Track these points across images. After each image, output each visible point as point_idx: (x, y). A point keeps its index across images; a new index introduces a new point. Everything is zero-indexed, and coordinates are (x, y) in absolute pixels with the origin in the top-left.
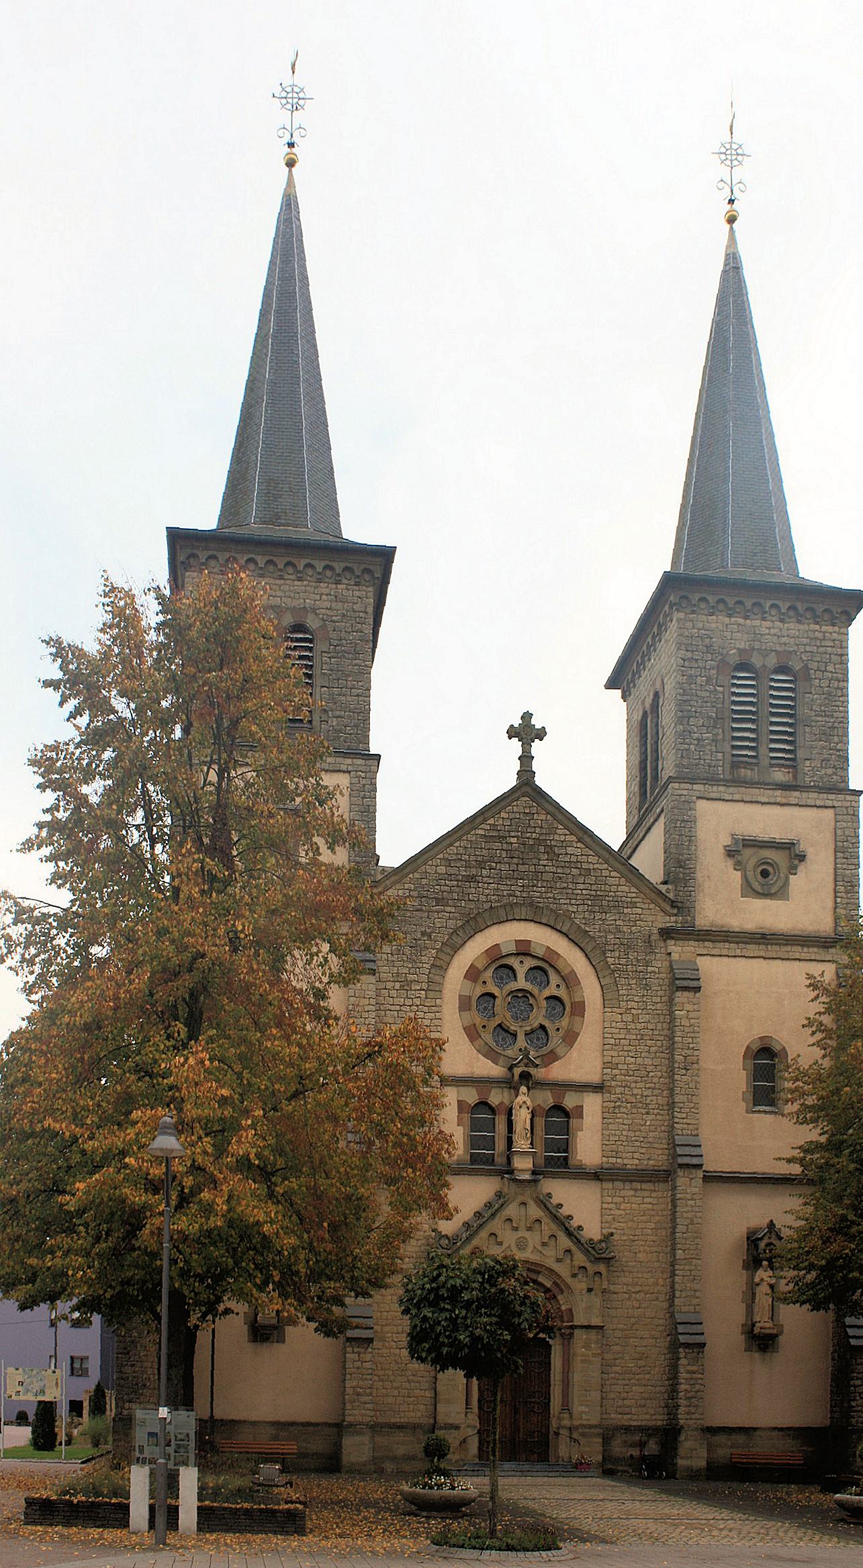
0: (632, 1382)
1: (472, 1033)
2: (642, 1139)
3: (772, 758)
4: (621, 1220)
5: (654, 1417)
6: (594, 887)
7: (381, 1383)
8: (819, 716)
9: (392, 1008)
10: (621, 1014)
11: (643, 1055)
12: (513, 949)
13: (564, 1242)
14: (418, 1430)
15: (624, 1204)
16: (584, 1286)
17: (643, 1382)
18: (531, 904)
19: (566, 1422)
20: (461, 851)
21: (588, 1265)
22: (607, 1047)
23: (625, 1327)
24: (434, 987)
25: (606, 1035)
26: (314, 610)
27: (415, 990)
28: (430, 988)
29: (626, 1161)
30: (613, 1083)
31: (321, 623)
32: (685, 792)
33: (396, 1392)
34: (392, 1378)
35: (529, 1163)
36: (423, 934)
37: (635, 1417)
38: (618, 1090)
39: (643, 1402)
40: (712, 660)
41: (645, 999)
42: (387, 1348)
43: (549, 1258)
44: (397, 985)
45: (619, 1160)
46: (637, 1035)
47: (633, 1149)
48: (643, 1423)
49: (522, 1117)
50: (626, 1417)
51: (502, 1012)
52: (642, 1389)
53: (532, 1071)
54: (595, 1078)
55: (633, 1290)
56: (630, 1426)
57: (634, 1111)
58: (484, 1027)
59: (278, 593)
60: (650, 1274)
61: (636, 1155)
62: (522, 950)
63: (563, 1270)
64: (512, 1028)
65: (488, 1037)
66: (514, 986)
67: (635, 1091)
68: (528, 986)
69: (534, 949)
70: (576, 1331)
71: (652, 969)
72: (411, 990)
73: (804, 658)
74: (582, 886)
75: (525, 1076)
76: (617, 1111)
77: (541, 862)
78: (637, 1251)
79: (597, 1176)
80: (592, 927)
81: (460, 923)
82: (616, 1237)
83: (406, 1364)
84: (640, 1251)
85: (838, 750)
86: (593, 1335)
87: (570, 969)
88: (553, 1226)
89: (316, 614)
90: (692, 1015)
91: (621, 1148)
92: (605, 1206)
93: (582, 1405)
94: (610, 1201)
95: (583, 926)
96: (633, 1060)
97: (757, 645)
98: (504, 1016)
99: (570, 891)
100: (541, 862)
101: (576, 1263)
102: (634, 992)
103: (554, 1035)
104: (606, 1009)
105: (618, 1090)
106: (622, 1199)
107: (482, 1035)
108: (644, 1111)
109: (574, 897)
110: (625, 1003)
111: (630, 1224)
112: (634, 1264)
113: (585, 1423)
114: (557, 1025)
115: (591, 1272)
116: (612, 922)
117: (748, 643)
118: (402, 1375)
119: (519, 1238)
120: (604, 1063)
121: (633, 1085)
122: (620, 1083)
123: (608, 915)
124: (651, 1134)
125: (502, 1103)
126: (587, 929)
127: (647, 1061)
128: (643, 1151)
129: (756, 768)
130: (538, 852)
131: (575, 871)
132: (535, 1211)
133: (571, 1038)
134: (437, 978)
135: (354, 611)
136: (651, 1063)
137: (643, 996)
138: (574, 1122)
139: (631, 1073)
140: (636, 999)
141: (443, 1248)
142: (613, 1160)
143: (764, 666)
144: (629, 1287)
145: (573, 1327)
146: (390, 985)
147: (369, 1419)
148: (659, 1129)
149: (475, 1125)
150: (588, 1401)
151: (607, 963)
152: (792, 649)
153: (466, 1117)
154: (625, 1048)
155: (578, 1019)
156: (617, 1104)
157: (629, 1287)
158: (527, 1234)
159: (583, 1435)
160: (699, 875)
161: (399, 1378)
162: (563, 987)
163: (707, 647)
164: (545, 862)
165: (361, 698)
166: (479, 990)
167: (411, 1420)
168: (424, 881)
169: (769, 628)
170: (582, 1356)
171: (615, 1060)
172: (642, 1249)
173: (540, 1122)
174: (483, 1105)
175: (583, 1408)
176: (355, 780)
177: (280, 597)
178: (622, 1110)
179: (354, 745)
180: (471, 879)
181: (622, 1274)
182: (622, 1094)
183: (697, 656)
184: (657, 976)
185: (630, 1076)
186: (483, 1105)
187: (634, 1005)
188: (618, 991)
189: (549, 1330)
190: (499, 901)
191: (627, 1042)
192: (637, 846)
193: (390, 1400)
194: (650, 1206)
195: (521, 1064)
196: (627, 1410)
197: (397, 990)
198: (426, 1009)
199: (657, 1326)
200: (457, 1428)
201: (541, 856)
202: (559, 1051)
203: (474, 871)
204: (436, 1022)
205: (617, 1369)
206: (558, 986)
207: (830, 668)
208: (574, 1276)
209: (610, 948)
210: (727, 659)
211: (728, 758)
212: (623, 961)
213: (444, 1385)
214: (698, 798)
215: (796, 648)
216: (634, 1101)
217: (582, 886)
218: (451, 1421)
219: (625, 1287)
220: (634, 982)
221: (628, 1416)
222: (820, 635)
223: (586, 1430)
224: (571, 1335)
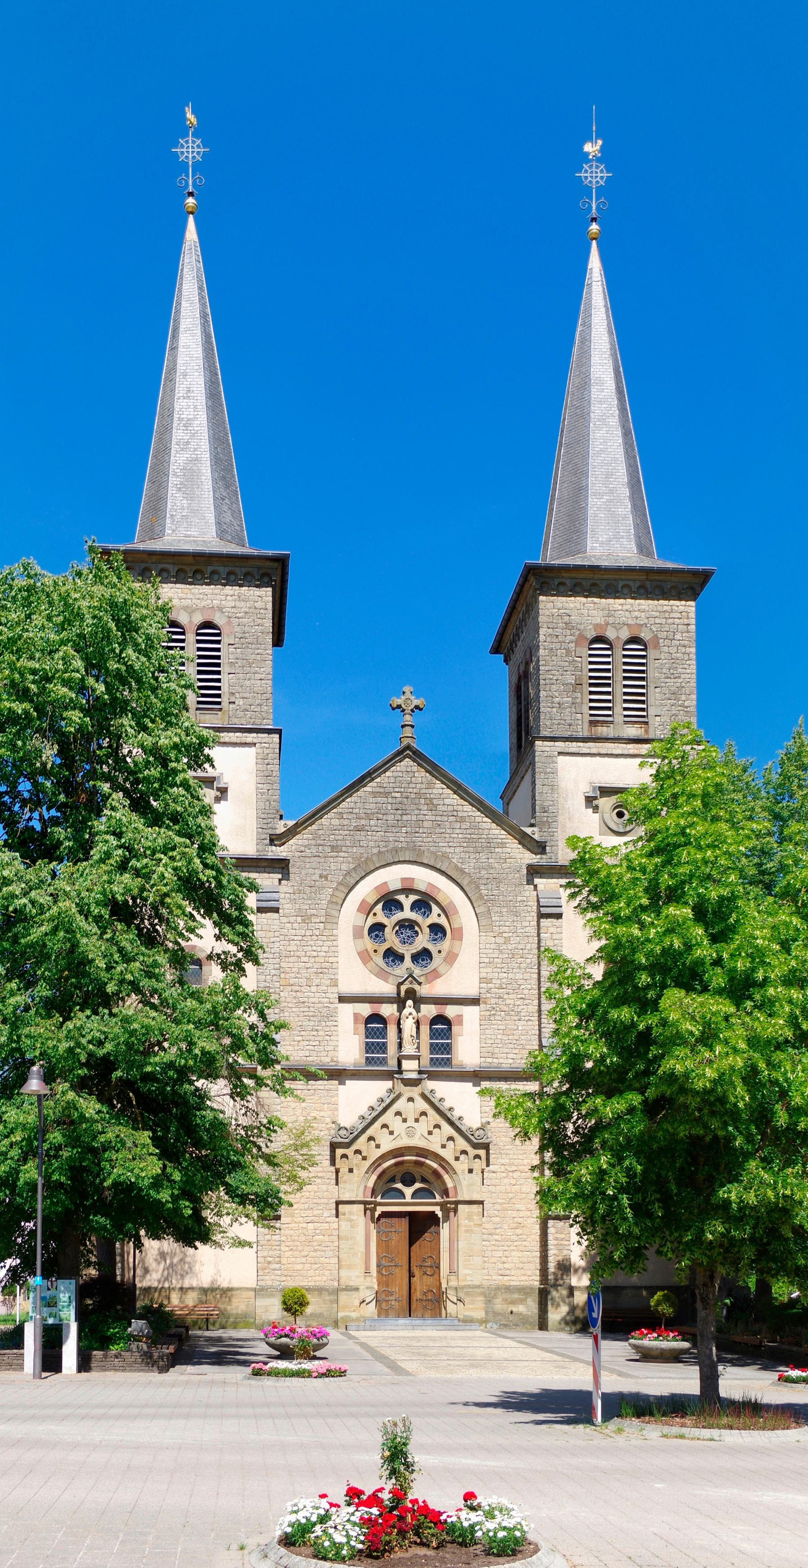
1: (365, 956)
3: (626, 716)
5: (531, 1278)
6: (469, 831)
7: (291, 1253)
8: (668, 678)
9: (296, 938)
11: (515, 971)
12: (399, 886)
13: (448, 1130)
14: (324, 1292)
16: (466, 1167)
17: (521, 1248)
18: (414, 849)
19: (453, 1283)
20: (352, 805)
22: (482, 965)
24: (331, 920)
25: (482, 955)
26: (220, 609)
29: (501, 1061)
30: (488, 995)
31: (227, 620)
32: (548, 749)
33: (304, 1260)
36: (321, 876)
37: (514, 1278)
38: (493, 1001)
40: (571, 635)
43: (434, 1144)
44: (299, 919)
45: (495, 1060)
48: (522, 1283)
49: (409, 1026)
50: (506, 1278)
51: (392, 939)
53: (416, 987)
54: (472, 991)
58: (375, 951)
59: (190, 596)
61: (510, 1056)
62: (407, 886)
63: (448, 1154)
64: (400, 951)
65: (379, 959)
66: (399, 916)
67: (508, 1002)
70: (460, 1206)
73: (654, 629)
74: (458, 831)
75: (411, 994)
76: (492, 1018)
77: (422, 812)
79: (476, 1076)
81: (352, 866)
85: (687, 707)
86: (476, 1208)
87: (448, 901)
89: (222, 612)
90: (555, 936)
91: (497, 1050)
95: (459, 865)
96: (505, 975)
97: (611, 620)
99: (447, 836)
100: (422, 812)
105: (493, 1001)
107: (374, 958)
108: (516, 1018)
109: (451, 840)
110: (497, 928)
113: (470, 1283)
114: (439, 948)
117: (603, 619)
121: (506, 996)
124: (523, 1037)
127: (519, 976)
128: (515, 1051)
129: (612, 725)
130: (419, 804)
131: (452, 819)
132: (422, 1105)
133: (451, 958)
134: (334, 913)
135: (255, 608)
136: (521, 977)
140: (507, 924)
142: (490, 1060)
143: (618, 638)
145: (457, 1203)
146: (292, 919)
147: (278, 1283)
149: (369, 1033)
152: (642, 622)
155: (457, 943)
159: (467, 1294)
160: (560, 818)
163: (566, 623)
164: (425, 812)
165: (263, 682)
166: (371, 921)
167: (317, 1284)
168: (321, 832)
169: (622, 605)
171: (490, 976)
173: (425, 1029)
174: (375, 1018)
175: (467, 1271)
176: (260, 751)
177: (191, 599)
178: (497, 1018)
179: (258, 721)
180: (358, 829)
183: (558, 631)
186: (375, 1018)
189: (306, 1145)
190: (386, 846)
191: (499, 961)
192: (516, 791)
193: (300, 1267)
195: (407, 982)
200: (357, 1289)
201: (421, 807)
202: (441, 970)
203: (363, 822)
204: (333, 949)
207: (678, 637)
208: (457, 1159)
210: (584, 633)
211: (587, 718)
214: (560, 753)
215: (646, 621)
217: (458, 831)
218: (351, 1283)
220: (505, 910)
222: (668, 608)
224: (456, 1211)
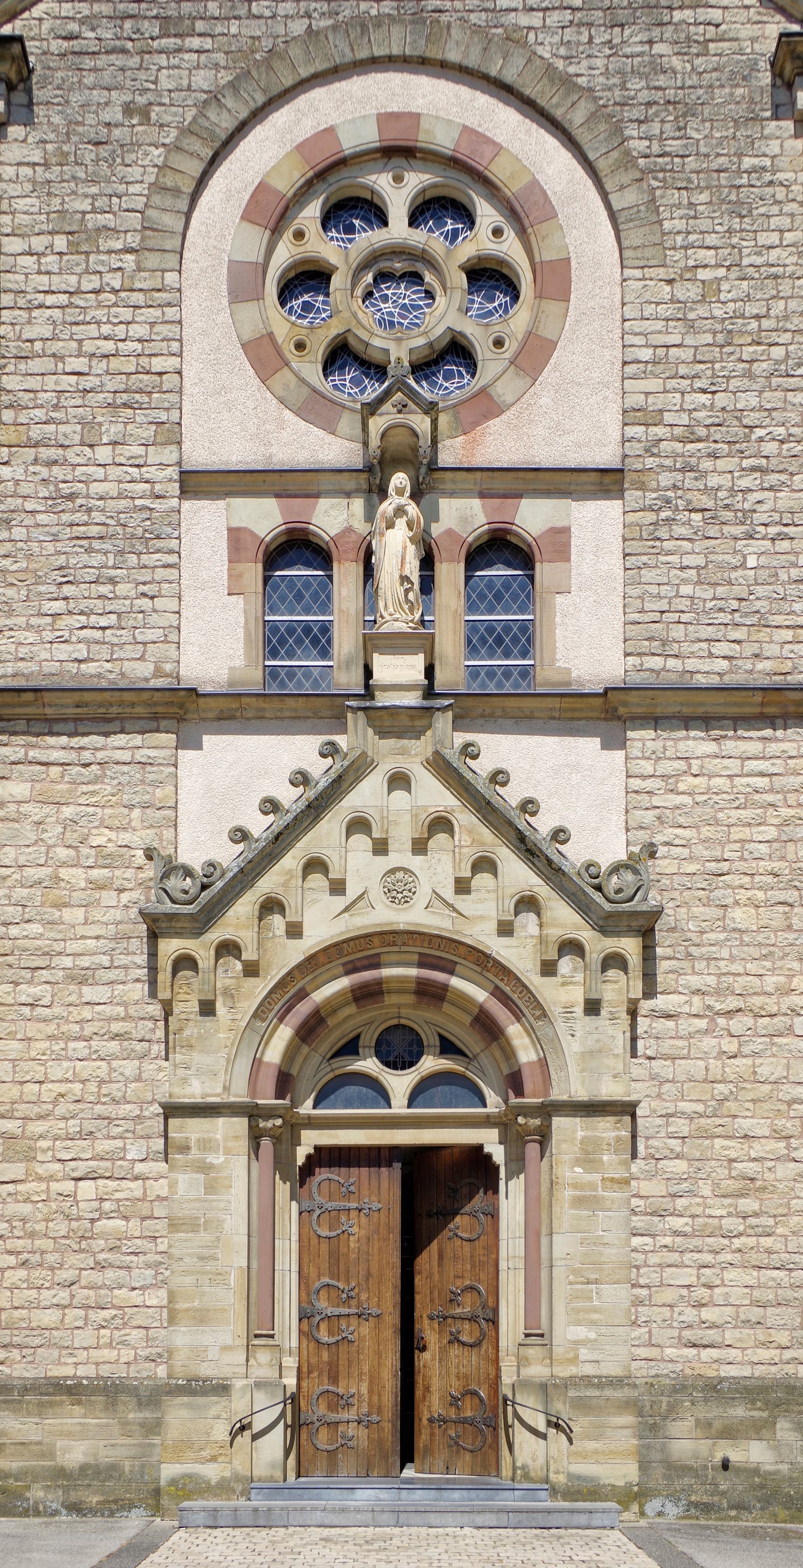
0: (722, 1257)
2: (735, 604)
4: (682, 820)
7: (22, 1273)
9: (50, 300)
10: (670, 282)
15: (690, 779)
16: (577, 995)
17: (755, 1258)
19: (537, 1371)
21: (586, 935)
22: (630, 369)
23: (700, 1108)
27: (110, 252)
28: (150, 244)
29: (692, 664)
30: (650, 462)
34: (51, 1258)
35: (413, 667)
36: (128, 110)
38: (666, 480)
39: (755, 1313)
41: (735, 240)
42: (40, 1179)
44: (60, 243)
45: (672, 663)
46: (715, 333)
47: (709, 633)
48: (759, 1371)
50: (707, 1354)
52: (751, 1277)
55: (718, 1006)
56: (722, 1380)
57: (713, 531)
60: (768, 964)
67: (713, 481)
68: (418, 237)
69: (427, 132)
70: (558, 1122)
71: (756, 161)
72: (99, 252)
78: (729, 901)
80: (585, 63)
81: (225, 77)
82: (663, 864)
83: (93, 1221)
84: (737, 903)
87: (525, 180)
88: (486, 834)
91: (678, 632)
92: (636, 784)
93: (578, 1323)
94: (650, 770)
95: (560, 64)
96: (704, 398)
98: (355, 315)
101: (555, 933)
102: (704, 224)
103: (489, 355)
104: (628, 272)
105: (666, 480)
106: (681, 765)
108: (738, 530)
110: (678, 255)
111: (706, 832)
112: (722, 936)
114: (497, 329)
115: (594, 955)
116: (638, 49)
118: (82, 1251)
119: (393, 871)
120: (625, 411)
121: (707, 464)
122: (668, 462)
123: (627, 32)
124: (760, 591)
125: (349, 530)
126: (572, 70)
137: (729, 231)
138: (543, 571)
139: (702, 432)
140: (711, 240)
141: (173, 901)
142: (656, 662)
144: (710, 1001)
146: (38, 243)
148: (783, 576)
150: (596, 1310)
151: (627, 153)
153: (254, 571)
154: (683, 369)
155: (551, 307)
156: (663, 515)
157: (710, 1001)
158: (415, 863)
161: (73, 1259)
162: (510, 234)
170: (575, 1186)
172: (742, 895)
175: (581, 1332)
178: (679, 531)
181: (686, 964)
182: (675, 487)
184: (768, 177)
185: (699, 440)
187: (708, 256)
188: (660, 222)
193: (50, 1317)
194: (761, 782)
196: (712, 1335)
197: (60, 254)
198: (138, 298)
199: (789, 1103)
200: (223, 1389)
205: (678, 1223)
206: (497, 232)
209: (636, 114)
212: (673, 146)
213: (186, 1273)
216: (710, 504)
218: (206, 1370)
219: (696, 999)
220: (704, 197)
221: (714, 1353)
223: (590, 1393)
224: (544, 1137)
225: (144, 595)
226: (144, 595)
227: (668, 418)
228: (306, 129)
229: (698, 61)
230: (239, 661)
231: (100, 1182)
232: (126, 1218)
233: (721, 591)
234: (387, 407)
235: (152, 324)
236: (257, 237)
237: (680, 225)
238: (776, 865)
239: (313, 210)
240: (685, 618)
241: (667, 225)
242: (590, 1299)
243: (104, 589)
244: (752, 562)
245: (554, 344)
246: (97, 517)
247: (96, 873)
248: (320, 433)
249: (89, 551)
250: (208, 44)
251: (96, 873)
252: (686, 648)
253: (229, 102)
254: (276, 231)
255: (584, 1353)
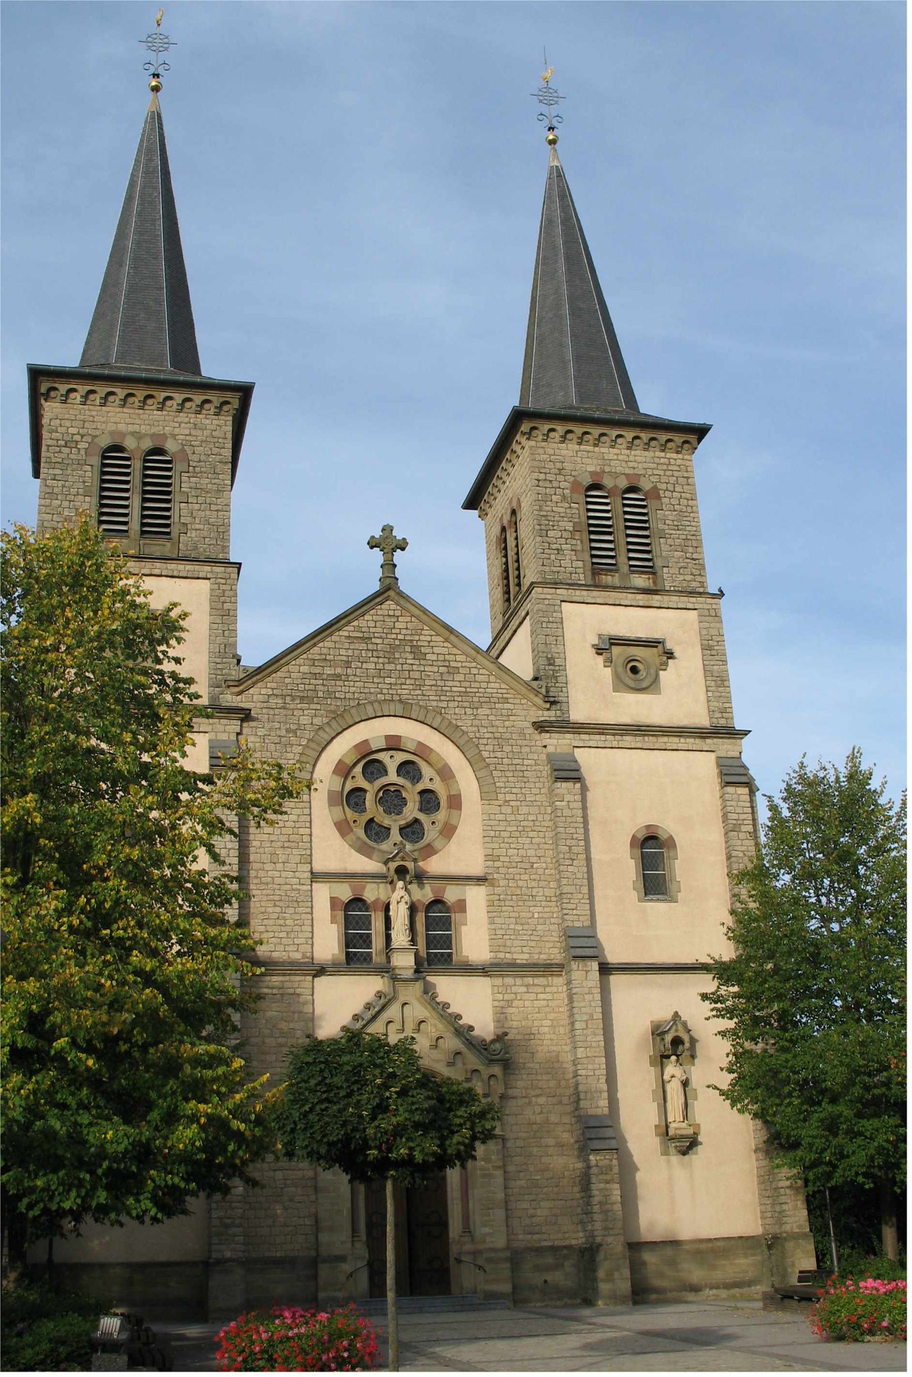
19: (468, 1247)
45: (508, 955)
50: (536, 1237)
81: (325, 720)
93: (485, 1226)
101: (470, 1067)
124: (539, 927)
140: (514, 790)
142: (501, 955)
153: (340, 915)
154: (506, 840)
194: (545, 1003)
218: (337, 1252)
225: (297, 925)
226: (297, 925)
227: (502, 859)
228: (358, 740)
229: (507, 723)
230: (336, 951)
231: (285, 1172)
232: (296, 1187)
233: (525, 927)
234: (397, 858)
235: (299, 815)
236: (338, 781)
237: (502, 785)
238: (552, 1036)
239: (359, 769)
240: (512, 937)
241: (498, 784)
242: (489, 1215)
243: (281, 922)
244: (536, 915)
245: (456, 828)
246: (277, 892)
247: (280, 1040)
248: (367, 859)
249: (275, 906)
250: (318, 707)
251: (280, 1040)
252: (513, 949)
253: (327, 729)
254: (346, 778)
255: (488, 1239)
